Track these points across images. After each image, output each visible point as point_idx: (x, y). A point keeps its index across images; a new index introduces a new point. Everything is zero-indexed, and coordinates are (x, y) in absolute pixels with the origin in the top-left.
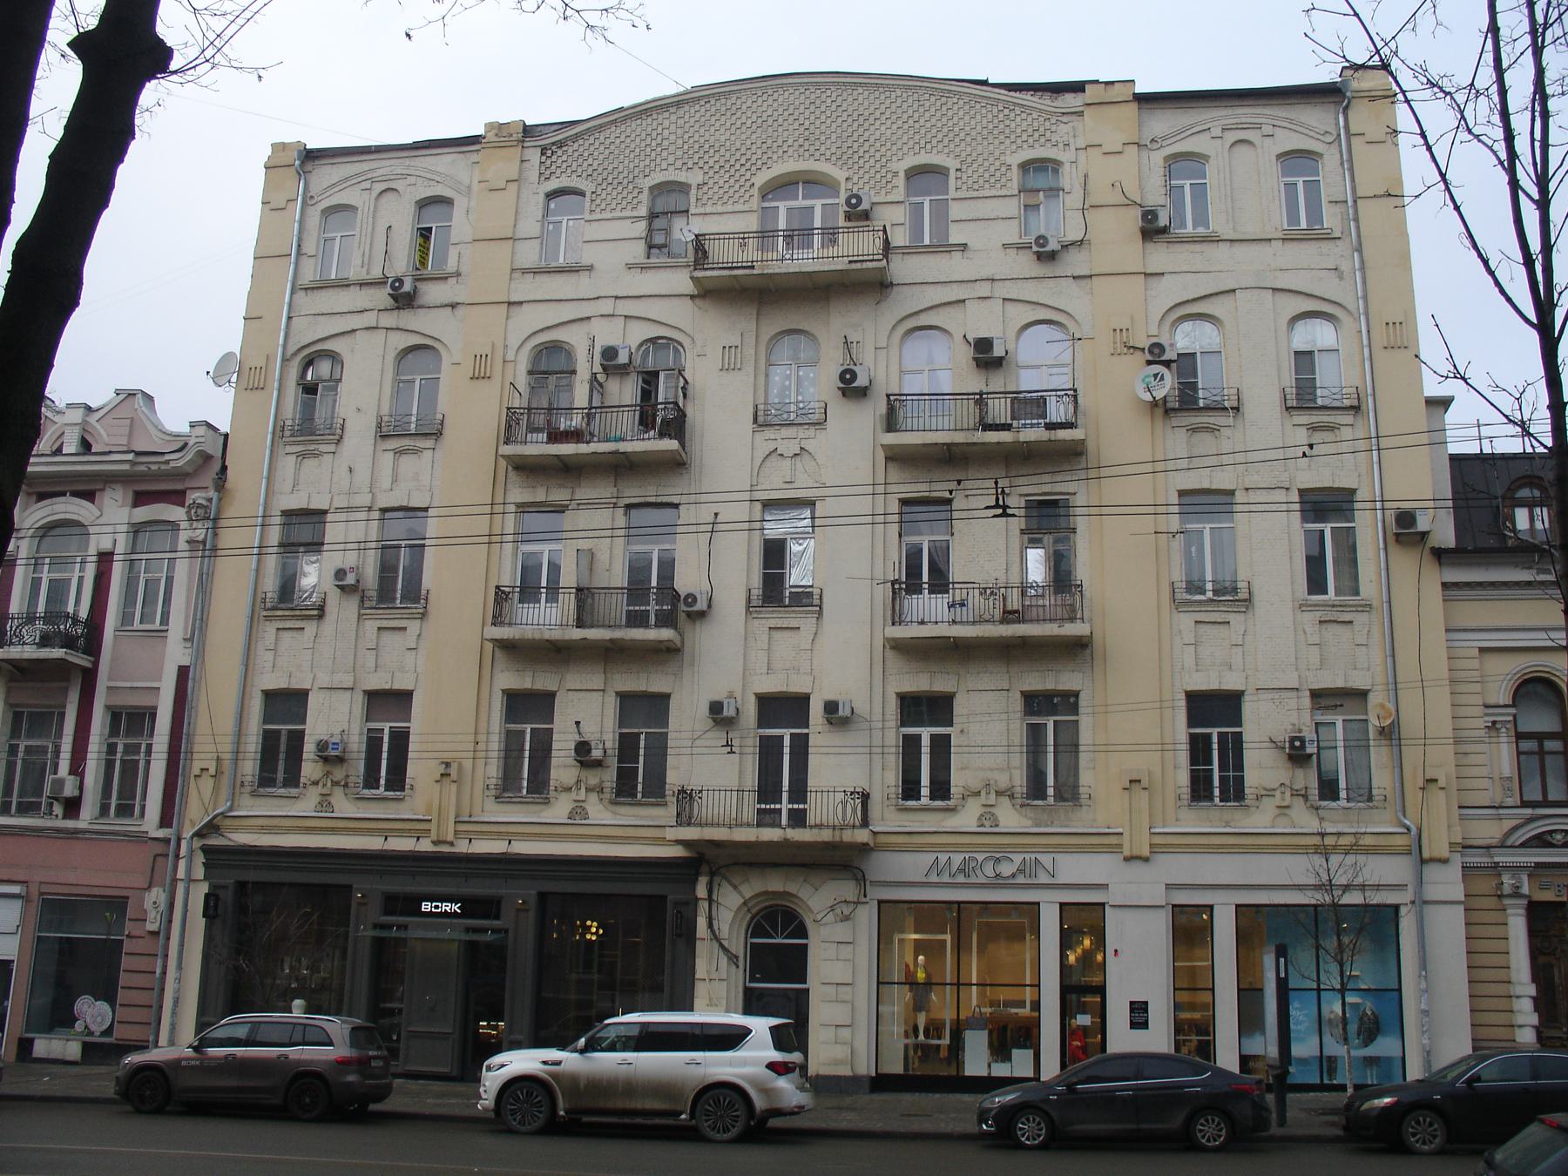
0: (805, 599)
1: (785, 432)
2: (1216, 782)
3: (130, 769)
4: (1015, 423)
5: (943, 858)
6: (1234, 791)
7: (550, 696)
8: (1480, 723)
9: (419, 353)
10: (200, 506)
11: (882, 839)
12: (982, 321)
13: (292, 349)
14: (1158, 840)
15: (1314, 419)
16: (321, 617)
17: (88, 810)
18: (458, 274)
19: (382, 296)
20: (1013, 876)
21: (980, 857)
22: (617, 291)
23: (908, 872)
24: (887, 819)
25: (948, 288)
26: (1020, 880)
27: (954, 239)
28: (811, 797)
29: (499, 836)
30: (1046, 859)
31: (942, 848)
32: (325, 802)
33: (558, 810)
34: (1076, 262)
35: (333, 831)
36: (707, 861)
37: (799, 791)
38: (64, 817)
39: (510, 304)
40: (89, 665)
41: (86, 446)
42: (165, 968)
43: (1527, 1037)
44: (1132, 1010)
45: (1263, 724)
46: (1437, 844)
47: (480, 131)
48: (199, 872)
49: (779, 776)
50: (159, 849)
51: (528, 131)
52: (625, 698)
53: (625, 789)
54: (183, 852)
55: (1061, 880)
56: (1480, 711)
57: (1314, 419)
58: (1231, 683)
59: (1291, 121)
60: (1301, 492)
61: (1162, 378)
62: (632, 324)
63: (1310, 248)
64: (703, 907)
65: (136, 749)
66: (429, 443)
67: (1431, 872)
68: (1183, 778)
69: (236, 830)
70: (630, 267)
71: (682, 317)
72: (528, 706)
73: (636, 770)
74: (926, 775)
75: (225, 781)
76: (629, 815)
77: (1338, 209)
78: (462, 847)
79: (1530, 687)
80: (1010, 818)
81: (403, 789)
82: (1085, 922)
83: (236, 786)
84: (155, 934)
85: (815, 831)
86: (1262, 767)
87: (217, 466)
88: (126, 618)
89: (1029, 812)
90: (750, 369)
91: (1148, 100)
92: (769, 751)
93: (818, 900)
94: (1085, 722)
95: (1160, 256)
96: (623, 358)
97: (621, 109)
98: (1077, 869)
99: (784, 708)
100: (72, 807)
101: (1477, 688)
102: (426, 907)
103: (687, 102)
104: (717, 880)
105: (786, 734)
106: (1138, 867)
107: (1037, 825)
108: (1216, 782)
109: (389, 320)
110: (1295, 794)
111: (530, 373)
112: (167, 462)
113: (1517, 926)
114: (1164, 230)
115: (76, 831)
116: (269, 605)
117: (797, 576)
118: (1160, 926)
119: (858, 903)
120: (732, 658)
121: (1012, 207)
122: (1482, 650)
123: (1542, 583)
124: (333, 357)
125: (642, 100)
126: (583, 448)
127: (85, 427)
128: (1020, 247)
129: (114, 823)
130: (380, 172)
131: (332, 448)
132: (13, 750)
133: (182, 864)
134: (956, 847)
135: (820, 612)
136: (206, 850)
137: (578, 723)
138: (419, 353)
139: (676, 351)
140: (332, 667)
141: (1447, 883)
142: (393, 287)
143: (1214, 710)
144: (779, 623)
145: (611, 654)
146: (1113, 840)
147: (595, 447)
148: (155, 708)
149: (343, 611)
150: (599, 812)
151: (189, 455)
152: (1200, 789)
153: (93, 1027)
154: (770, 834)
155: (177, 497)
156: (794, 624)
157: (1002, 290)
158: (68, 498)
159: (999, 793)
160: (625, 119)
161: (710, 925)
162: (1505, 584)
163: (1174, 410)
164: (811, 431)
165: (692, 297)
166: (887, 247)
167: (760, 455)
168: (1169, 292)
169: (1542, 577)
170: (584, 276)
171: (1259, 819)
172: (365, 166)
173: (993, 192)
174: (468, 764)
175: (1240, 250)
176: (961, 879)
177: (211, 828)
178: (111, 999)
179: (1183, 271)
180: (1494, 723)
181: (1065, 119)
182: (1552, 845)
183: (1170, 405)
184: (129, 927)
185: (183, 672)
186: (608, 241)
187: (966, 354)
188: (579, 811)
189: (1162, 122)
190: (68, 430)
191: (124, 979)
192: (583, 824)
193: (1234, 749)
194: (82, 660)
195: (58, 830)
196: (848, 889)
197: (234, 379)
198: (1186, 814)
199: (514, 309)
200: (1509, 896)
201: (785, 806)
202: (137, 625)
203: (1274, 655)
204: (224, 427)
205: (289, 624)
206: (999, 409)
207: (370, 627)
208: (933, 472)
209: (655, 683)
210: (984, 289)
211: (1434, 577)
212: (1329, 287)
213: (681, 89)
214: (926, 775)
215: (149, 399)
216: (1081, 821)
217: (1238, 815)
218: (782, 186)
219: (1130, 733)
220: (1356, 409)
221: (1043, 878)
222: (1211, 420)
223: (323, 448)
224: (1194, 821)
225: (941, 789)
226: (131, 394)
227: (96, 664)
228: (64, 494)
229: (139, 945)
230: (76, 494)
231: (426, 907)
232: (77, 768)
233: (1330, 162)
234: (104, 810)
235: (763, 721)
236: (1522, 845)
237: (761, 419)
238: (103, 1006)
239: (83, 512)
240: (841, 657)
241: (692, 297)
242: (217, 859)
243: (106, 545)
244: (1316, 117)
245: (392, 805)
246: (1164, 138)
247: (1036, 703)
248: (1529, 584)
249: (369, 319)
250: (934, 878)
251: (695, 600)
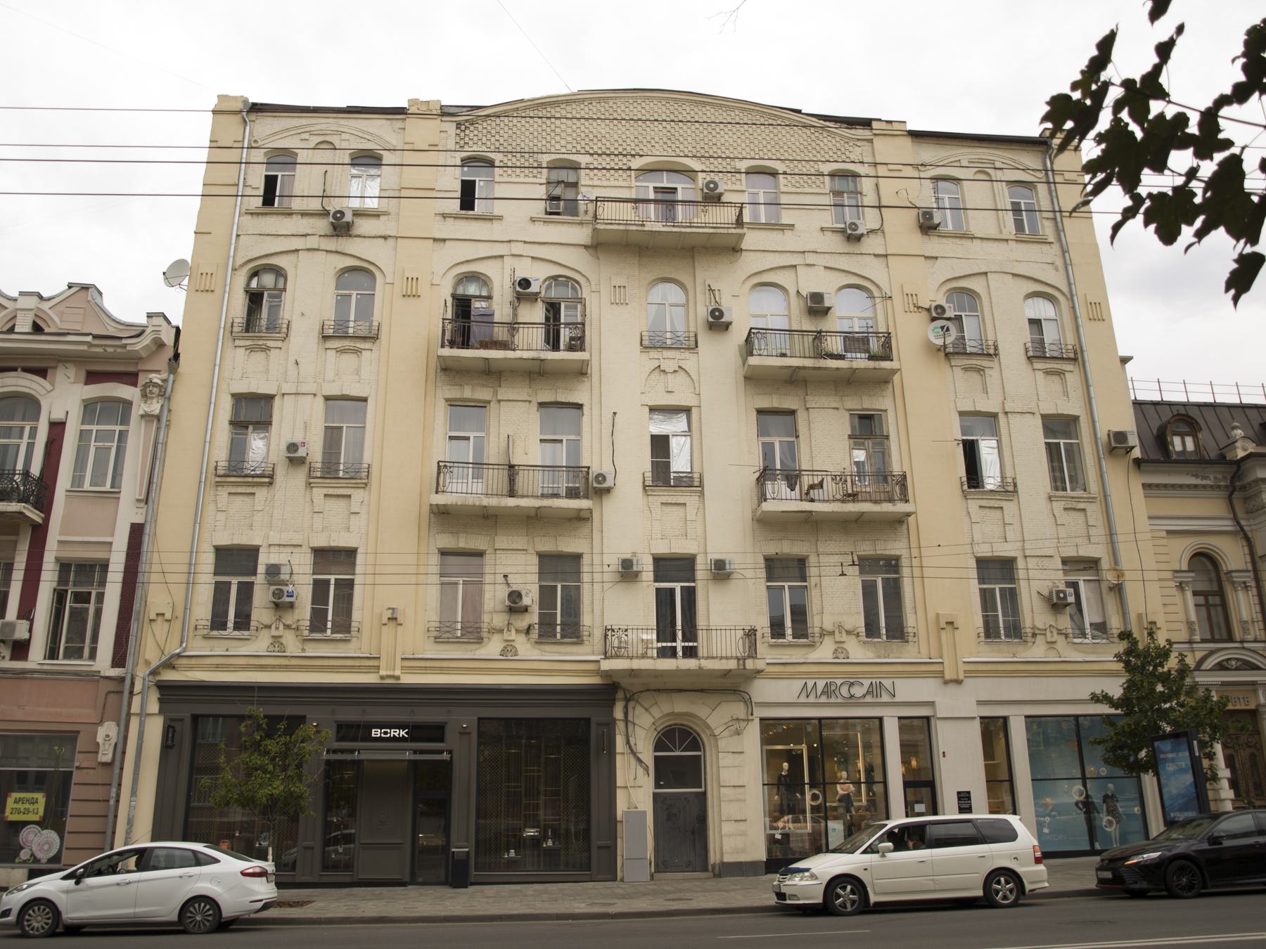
0: (690, 482)
1: (667, 354)
2: (1001, 625)
3: (79, 618)
4: (849, 355)
5: (810, 683)
9: (358, 275)
10: (155, 385)
12: (811, 282)
13: (240, 261)
15: (1048, 366)
16: (271, 483)
19: (323, 225)
20: (864, 696)
21: (839, 682)
22: (519, 240)
23: (780, 695)
25: (784, 256)
26: (869, 699)
27: (784, 221)
28: (701, 635)
30: (887, 683)
31: (809, 675)
33: (492, 648)
34: (872, 244)
35: (287, 668)
36: (609, 691)
37: (691, 632)
38: (12, 659)
40: (40, 521)
41: (37, 329)
42: (118, 795)
44: (959, 799)
45: (1037, 581)
47: (405, 105)
48: (154, 707)
49: (676, 618)
50: (112, 686)
52: (542, 556)
53: (546, 632)
54: (137, 688)
55: (897, 699)
57: (1048, 366)
60: (1044, 417)
61: (948, 330)
63: (1035, 248)
64: (620, 726)
65: (85, 598)
68: (979, 622)
70: (533, 220)
71: (578, 261)
73: (560, 619)
74: (792, 622)
76: (553, 653)
78: (409, 679)
79: (1203, 559)
80: (858, 652)
81: (349, 632)
82: (919, 733)
84: (105, 764)
85: (724, 661)
86: (1033, 613)
87: (171, 353)
88: (77, 479)
91: (917, 135)
92: (664, 600)
93: (715, 717)
95: (933, 245)
96: (534, 288)
97: (522, 101)
98: (910, 690)
99: (674, 567)
100: (20, 649)
102: (376, 733)
103: (574, 101)
104: (631, 704)
106: (952, 688)
107: (879, 657)
109: (332, 244)
110: (1060, 632)
112: (124, 346)
114: (935, 227)
116: (221, 472)
117: (679, 462)
118: (974, 732)
119: (748, 720)
120: (631, 527)
122: (1169, 532)
123: (1204, 486)
124: (279, 272)
125: (545, 94)
126: (510, 354)
128: (834, 231)
129: (62, 662)
130: (318, 127)
131: (279, 344)
133: (136, 701)
134: (820, 675)
135: (702, 494)
137: (506, 576)
138: (358, 275)
139: (574, 288)
140: (286, 525)
142: (334, 217)
144: (670, 500)
145: (534, 521)
146: (375, 663)
147: (518, 354)
148: (108, 560)
149: (290, 484)
150: (526, 649)
151: (146, 340)
152: (990, 631)
153: (39, 855)
154: (667, 664)
155: (130, 378)
156: (681, 500)
158: (19, 373)
161: (628, 742)
164: (687, 354)
165: (586, 247)
166: (739, 222)
169: (1204, 482)
172: (304, 122)
173: (810, 190)
176: (823, 699)
178: (60, 830)
181: (859, 143)
183: (950, 350)
184: (79, 760)
185: (137, 532)
186: (516, 199)
187: (797, 306)
189: (929, 153)
190: (20, 314)
191: (72, 808)
193: (1011, 597)
194: (35, 516)
196: (739, 710)
197: (186, 282)
201: (679, 644)
202: (87, 487)
203: (1039, 531)
204: (177, 320)
205: (240, 490)
206: (835, 344)
207: (318, 493)
208: (779, 392)
209: (569, 545)
211: (1137, 482)
213: (568, 92)
214: (792, 622)
215: (100, 294)
216: (908, 654)
217: (1020, 648)
219: (943, 591)
221: (885, 698)
222: (979, 363)
223: (270, 344)
225: (801, 628)
226: (85, 288)
227: (47, 520)
228: (15, 369)
229: (92, 776)
230: (26, 370)
231: (376, 733)
232: (26, 612)
233: (1042, 189)
234: (52, 653)
237: (646, 343)
238: (52, 836)
239: (34, 386)
240: (719, 526)
241: (586, 247)
242: (170, 693)
243: (58, 415)
245: (341, 645)
247: (867, 564)
248: (1196, 486)
249: (312, 242)
250: (803, 699)
251: (604, 478)
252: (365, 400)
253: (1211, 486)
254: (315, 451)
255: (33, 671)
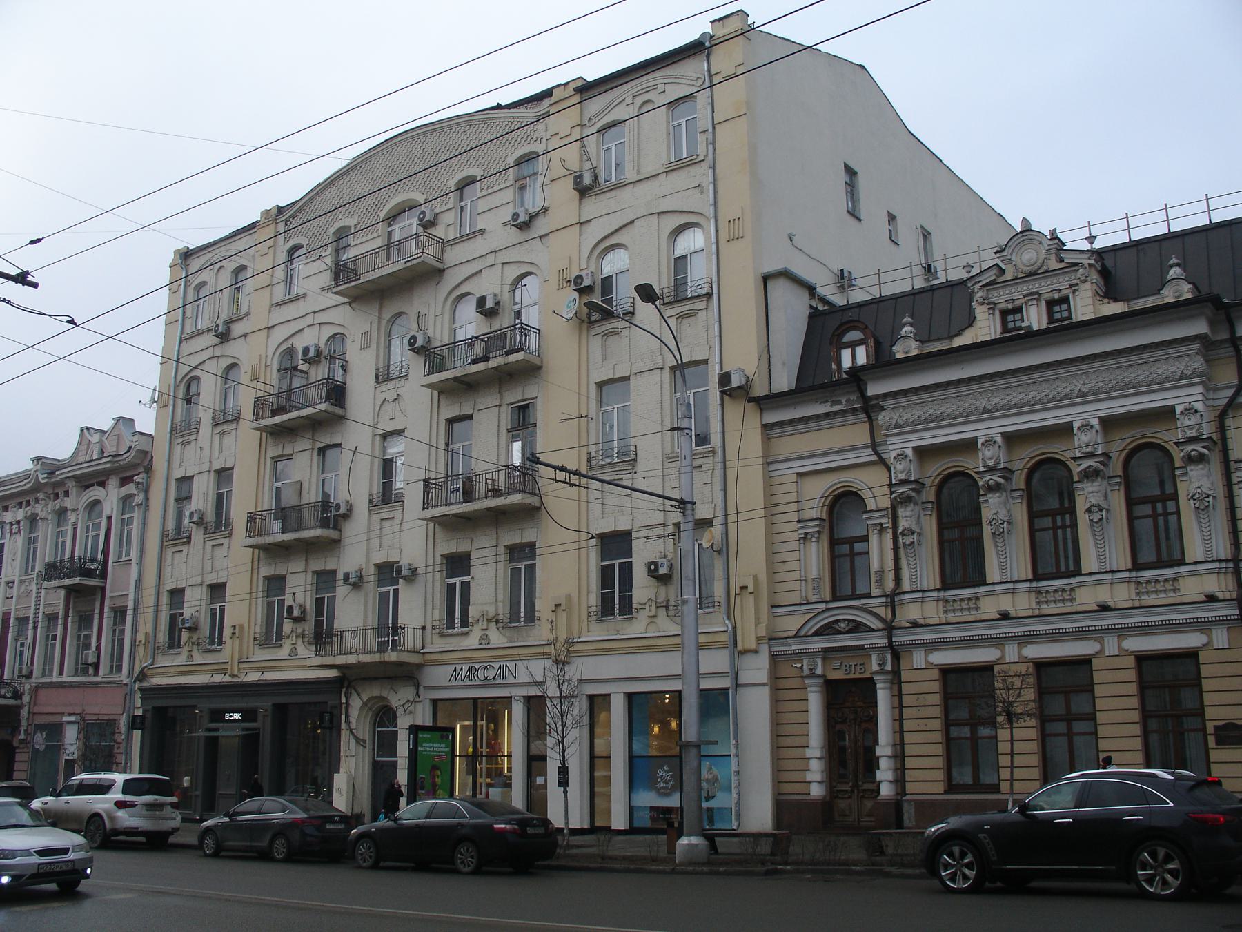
2: (617, 601)
5: (458, 668)
6: (627, 608)
7: (283, 578)
8: (795, 536)
11: (428, 657)
14: (702, 639)
16: (189, 542)
17: (103, 670)
18: (248, 314)
19: (210, 339)
24: (436, 644)
29: (257, 669)
30: (511, 665)
32: (190, 657)
33: (284, 652)
34: (541, 226)
36: (349, 678)
39: (269, 328)
43: (817, 791)
45: (643, 553)
46: (747, 640)
51: (280, 210)
56: (794, 526)
58: (623, 525)
59: (675, 77)
62: (323, 327)
66: (233, 426)
67: (748, 661)
69: (153, 676)
72: (276, 584)
74: (456, 612)
75: (150, 646)
77: (704, 136)
79: (1134, 461)
83: (156, 648)
89: (506, 632)
90: (374, 346)
94: (538, 562)
95: (592, 207)
97: (319, 185)
101: (794, 507)
102: (227, 716)
105: (391, 589)
108: (617, 601)
109: (218, 352)
111: (279, 371)
113: (815, 703)
115: (98, 683)
121: (508, 195)
122: (800, 475)
123: (836, 413)
127: (101, 442)
131: (194, 437)
132: (79, 636)
136: (142, 689)
141: (757, 669)
143: (616, 544)
157: (502, 257)
158: (96, 487)
159: (489, 621)
160: (323, 189)
162: (808, 419)
163: (596, 321)
167: (379, 403)
168: (595, 232)
170: (301, 303)
171: (637, 627)
174: (246, 626)
175: (640, 188)
177: (142, 676)
179: (603, 213)
180: (806, 534)
182: (840, 633)
188: (294, 651)
192: (297, 662)
195: (91, 683)
198: (594, 626)
199: (584, 227)
200: (807, 677)
209: (529, 536)
210: (490, 260)
211: (754, 422)
212: (694, 202)
213: (345, 163)
214: (456, 612)
218: (392, 218)
220: (709, 296)
221: (511, 680)
224: (598, 632)
225: (465, 622)
228: (92, 485)
234: (61, 673)
235: (380, 583)
236: (816, 634)
244: (693, 68)
245: (217, 654)
246: (597, 115)
249: (208, 353)
252: (705, 362)
253: (844, 412)
254: (210, 517)
255: (101, 682)
